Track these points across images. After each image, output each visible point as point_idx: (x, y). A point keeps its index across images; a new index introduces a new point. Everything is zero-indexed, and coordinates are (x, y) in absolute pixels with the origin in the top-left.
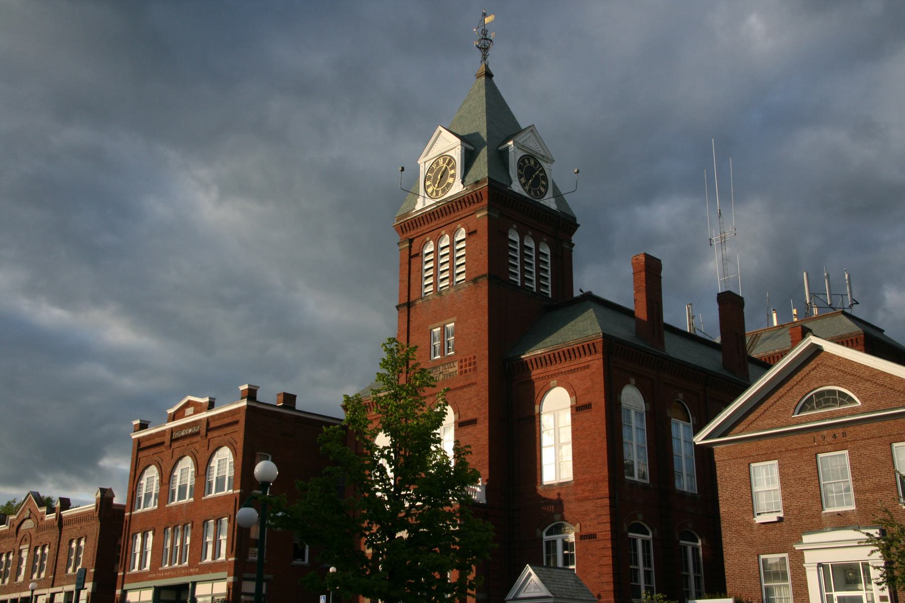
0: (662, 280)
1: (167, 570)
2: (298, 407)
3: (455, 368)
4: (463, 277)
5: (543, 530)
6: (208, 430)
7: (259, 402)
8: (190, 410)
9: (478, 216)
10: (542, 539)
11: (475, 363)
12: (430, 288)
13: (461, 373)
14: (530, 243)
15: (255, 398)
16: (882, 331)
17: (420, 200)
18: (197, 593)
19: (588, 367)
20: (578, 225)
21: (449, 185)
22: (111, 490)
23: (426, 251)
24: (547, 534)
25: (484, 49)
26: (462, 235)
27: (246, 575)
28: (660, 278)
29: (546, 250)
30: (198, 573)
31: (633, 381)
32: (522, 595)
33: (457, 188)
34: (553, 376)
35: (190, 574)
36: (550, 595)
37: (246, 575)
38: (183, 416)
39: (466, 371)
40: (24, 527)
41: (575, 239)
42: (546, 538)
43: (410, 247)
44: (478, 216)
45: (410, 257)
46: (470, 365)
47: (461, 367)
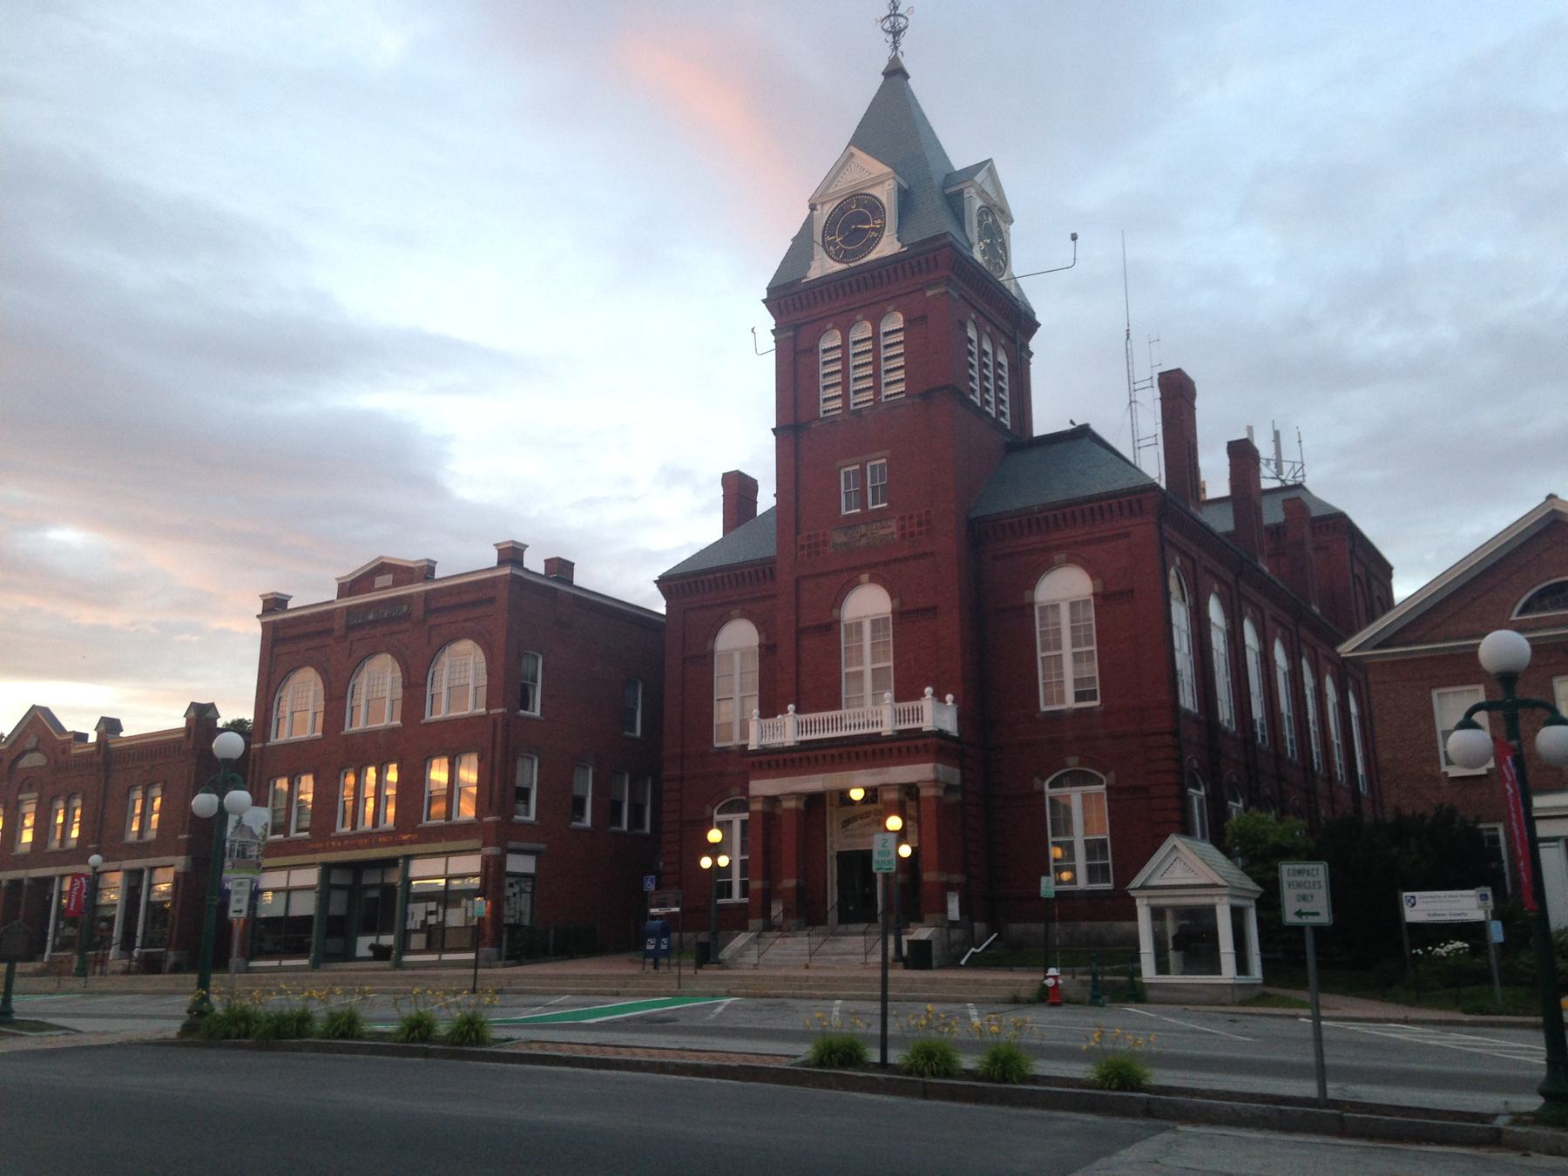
0: (1198, 413)
1: (347, 837)
2: (576, 582)
3: (891, 529)
4: (901, 387)
5: (1044, 779)
6: (428, 611)
7: (527, 571)
8: (381, 581)
9: (929, 293)
10: (1042, 793)
11: (929, 523)
12: (838, 403)
13: (903, 535)
14: (987, 347)
15: (521, 563)
16: (428, 571)
17: (814, 264)
18: (413, 872)
19: (1127, 535)
20: (1038, 325)
21: (874, 242)
22: (212, 705)
23: (824, 345)
24: (1052, 785)
25: (896, 33)
26: (895, 321)
27: (512, 845)
28: (1194, 409)
29: (1002, 359)
30: (411, 842)
31: (865, 577)
32: (1155, 882)
33: (888, 246)
34: (1059, 548)
35: (401, 843)
36: (1221, 882)
37: (512, 845)
38: (370, 589)
39: (912, 534)
40: (25, 762)
41: (1034, 344)
42: (1049, 792)
43: (795, 338)
44: (929, 293)
45: (796, 353)
46: (920, 525)
47: (903, 528)
